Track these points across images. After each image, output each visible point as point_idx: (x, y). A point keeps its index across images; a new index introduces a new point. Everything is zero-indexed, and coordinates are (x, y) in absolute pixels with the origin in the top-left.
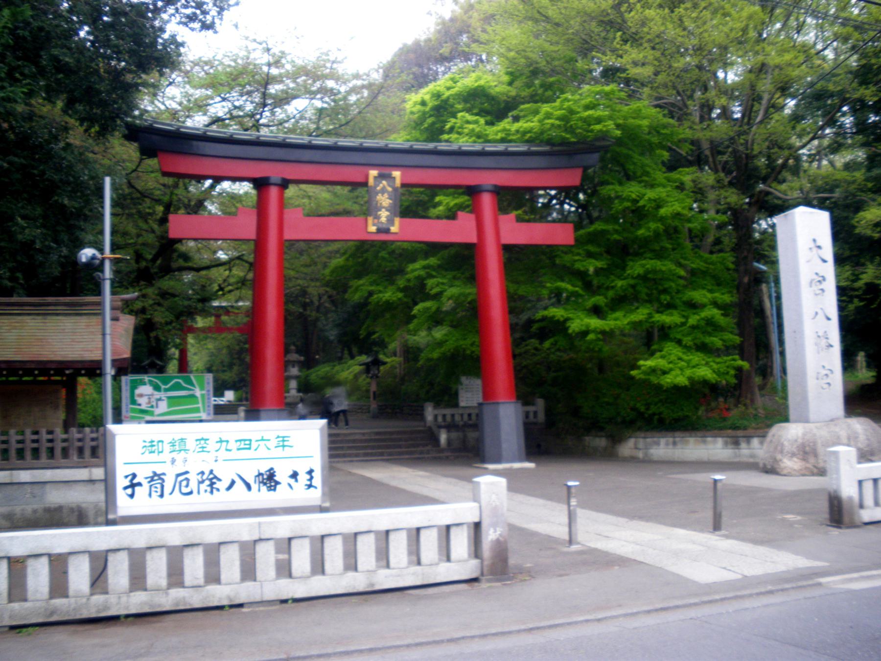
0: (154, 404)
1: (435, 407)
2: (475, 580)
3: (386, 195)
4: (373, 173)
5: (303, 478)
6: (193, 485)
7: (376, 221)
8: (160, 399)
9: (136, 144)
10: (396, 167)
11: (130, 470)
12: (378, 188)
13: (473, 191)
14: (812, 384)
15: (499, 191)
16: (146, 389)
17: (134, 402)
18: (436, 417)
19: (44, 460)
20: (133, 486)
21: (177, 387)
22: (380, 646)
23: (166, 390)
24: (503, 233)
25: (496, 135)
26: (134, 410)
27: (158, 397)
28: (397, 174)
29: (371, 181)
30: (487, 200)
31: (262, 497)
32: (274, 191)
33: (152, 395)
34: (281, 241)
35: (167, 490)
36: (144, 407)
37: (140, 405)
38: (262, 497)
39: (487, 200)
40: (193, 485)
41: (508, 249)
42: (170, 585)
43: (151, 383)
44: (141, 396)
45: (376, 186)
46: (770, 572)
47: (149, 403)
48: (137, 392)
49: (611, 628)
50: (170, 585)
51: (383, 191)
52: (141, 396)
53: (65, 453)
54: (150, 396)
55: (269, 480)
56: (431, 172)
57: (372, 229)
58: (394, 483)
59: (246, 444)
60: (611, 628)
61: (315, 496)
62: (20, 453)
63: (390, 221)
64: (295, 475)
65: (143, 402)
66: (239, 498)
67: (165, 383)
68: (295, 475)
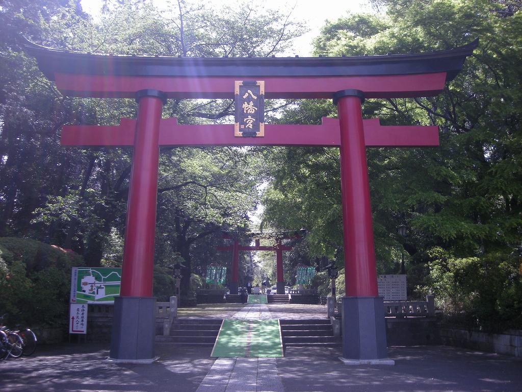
0: (96, 291)
3: (251, 103)
4: (238, 83)
7: (243, 127)
8: (100, 288)
9: (264, 81)
12: (244, 97)
16: (90, 279)
17: (80, 289)
23: (105, 280)
25: (131, 42)
26: (79, 296)
27: (99, 285)
28: (261, 83)
29: (237, 91)
33: (94, 283)
36: (87, 293)
37: (84, 291)
43: (94, 274)
44: (86, 284)
45: (242, 94)
47: (92, 290)
48: (83, 281)
49: (192, 312)
51: (249, 100)
52: (86, 284)
54: (92, 284)
60: (192, 312)
65: (87, 288)
67: (104, 275)
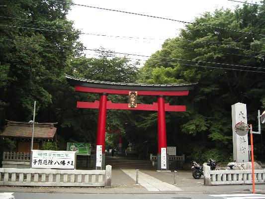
1: (153, 155)
2: (104, 187)
5: (71, 163)
6: (48, 162)
10: (136, 90)
11: (35, 159)
13: (101, 94)
14: (238, 151)
15: (164, 97)
18: (153, 158)
19: (24, 159)
20: (35, 162)
21: (82, 146)
22: (34, 185)
24: (165, 108)
28: (136, 92)
29: (129, 94)
30: (161, 99)
31: (62, 166)
32: (104, 96)
34: (106, 110)
35: (42, 163)
38: (62, 166)
39: (161, 99)
40: (48, 162)
41: (167, 113)
42: (16, 181)
44: (72, 148)
46: (161, 182)
48: (71, 147)
50: (16, 181)
52: (72, 148)
53: (26, 158)
55: (63, 163)
56: (168, 92)
57: (130, 107)
58: (127, 174)
59: (59, 155)
61: (73, 167)
62: (26, 158)
63: (134, 105)
64: (69, 162)
66: (57, 166)
68: (69, 162)
